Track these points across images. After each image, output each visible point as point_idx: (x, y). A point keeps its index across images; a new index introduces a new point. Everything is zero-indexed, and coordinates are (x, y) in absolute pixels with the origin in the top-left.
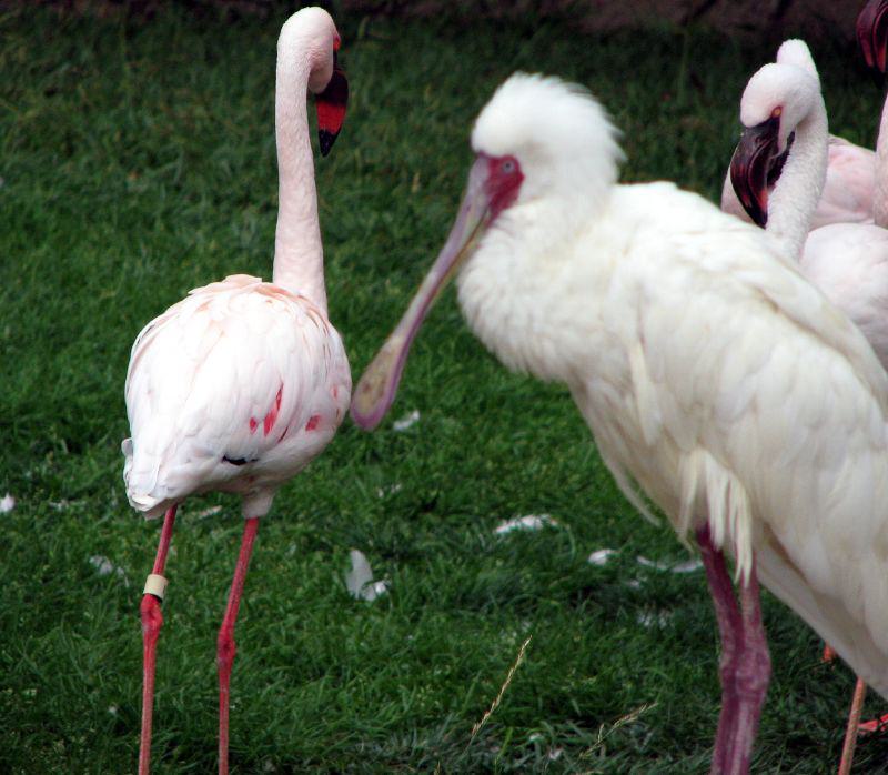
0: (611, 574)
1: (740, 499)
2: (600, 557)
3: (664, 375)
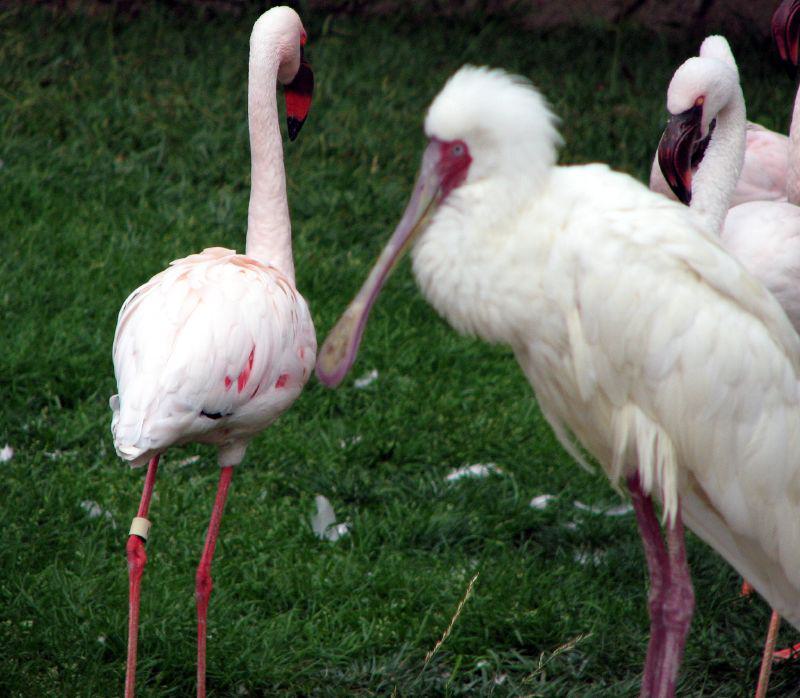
0: (551, 517)
1: (666, 449)
2: (540, 502)
3: (598, 338)
